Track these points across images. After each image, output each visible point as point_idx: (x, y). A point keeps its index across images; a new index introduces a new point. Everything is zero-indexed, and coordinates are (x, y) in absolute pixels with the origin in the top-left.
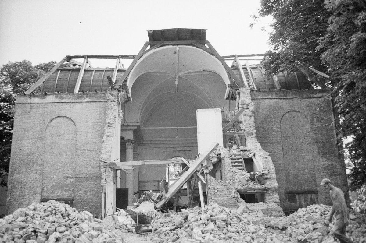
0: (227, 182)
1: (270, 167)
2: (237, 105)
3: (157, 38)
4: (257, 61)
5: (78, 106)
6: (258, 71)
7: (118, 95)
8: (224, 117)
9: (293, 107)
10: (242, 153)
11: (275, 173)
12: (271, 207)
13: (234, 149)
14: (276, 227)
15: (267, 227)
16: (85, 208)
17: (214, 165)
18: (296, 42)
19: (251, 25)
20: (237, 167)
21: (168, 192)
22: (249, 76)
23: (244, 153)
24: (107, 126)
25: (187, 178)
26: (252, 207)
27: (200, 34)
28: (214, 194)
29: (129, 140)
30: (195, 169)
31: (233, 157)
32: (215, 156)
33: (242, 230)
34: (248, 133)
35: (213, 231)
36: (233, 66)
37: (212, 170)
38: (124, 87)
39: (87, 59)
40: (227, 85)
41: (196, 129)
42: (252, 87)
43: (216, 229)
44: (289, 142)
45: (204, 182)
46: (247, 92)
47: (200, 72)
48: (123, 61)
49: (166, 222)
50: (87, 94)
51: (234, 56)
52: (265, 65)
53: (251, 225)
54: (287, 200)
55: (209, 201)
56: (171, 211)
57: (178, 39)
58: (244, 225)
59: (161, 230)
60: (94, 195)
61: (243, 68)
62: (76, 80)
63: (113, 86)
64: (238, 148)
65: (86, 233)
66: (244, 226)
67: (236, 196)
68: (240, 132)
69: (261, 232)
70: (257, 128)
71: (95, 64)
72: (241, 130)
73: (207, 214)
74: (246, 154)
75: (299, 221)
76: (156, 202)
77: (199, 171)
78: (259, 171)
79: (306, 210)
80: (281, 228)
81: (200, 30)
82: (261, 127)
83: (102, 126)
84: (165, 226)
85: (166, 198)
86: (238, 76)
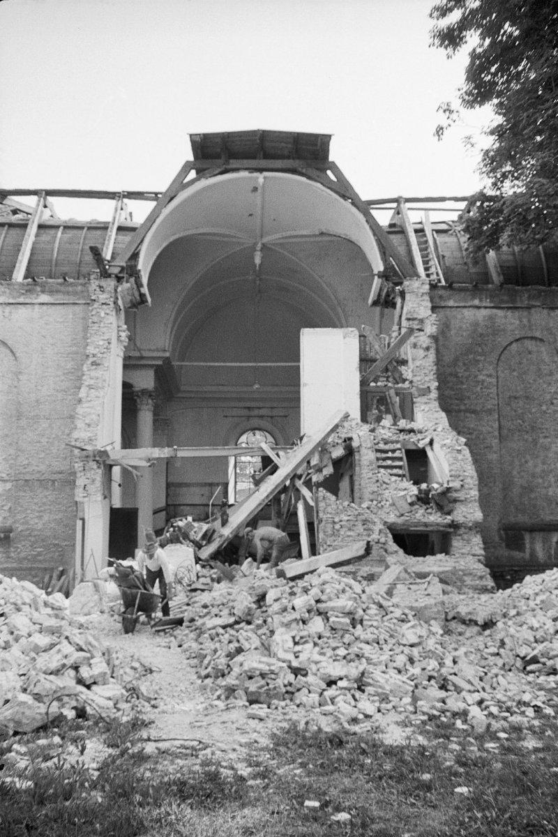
0: (365, 505)
1: (466, 474)
2: (396, 320)
3: (214, 152)
4: (450, 214)
5: (22, 311)
6: (449, 240)
7: (116, 290)
8: (365, 350)
9: (531, 329)
10: (402, 437)
11: (476, 488)
12: (463, 568)
13: (384, 427)
14: (470, 620)
15: (449, 618)
16: (39, 550)
17: (337, 463)
18: (543, 178)
19: (440, 131)
20: (389, 471)
21: (228, 524)
22: (429, 250)
23: (406, 437)
24: (89, 362)
25: (271, 493)
26: (421, 566)
27: (316, 145)
28: (333, 534)
29: (144, 392)
30: (292, 471)
31: (382, 446)
32: (340, 441)
33: (387, 638)
34: (418, 389)
35: (320, 638)
36: (391, 226)
37: (331, 475)
38: (131, 271)
39: (45, 199)
40: (376, 272)
41: (299, 366)
42: (434, 277)
43: (328, 634)
44: (515, 411)
45: (312, 503)
46: (422, 291)
47: (315, 236)
48: (131, 204)
49: (215, 603)
50: (43, 286)
51: (396, 200)
52: (468, 227)
53: (409, 624)
54: (504, 545)
55: (321, 549)
56: (234, 566)
57: (261, 156)
58: (394, 624)
59: (204, 624)
60: (59, 522)
61: (416, 231)
62: (18, 249)
63: (105, 268)
64: (395, 424)
65: (23, 641)
66: (392, 626)
67: (383, 540)
68: (400, 385)
69: (431, 644)
70: (442, 377)
71: (65, 210)
72: (404, 381)
73: (309, 597)
74: (412, 440)
75: (525, 608)
76: (198, 546)
77: (300, 477)
78: (440, 481)
79: (543, 581)
80: (481, 622)
81: (316, 136)
82: (451, 374)
83: (81, 360)
84: (213, 614)
85: (221, 536)
86: (402, 250)
